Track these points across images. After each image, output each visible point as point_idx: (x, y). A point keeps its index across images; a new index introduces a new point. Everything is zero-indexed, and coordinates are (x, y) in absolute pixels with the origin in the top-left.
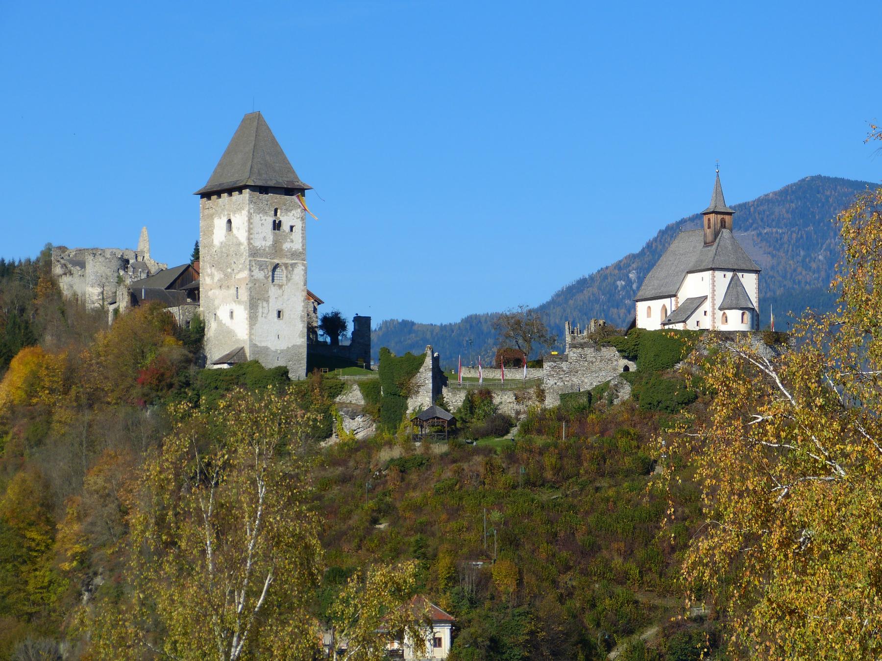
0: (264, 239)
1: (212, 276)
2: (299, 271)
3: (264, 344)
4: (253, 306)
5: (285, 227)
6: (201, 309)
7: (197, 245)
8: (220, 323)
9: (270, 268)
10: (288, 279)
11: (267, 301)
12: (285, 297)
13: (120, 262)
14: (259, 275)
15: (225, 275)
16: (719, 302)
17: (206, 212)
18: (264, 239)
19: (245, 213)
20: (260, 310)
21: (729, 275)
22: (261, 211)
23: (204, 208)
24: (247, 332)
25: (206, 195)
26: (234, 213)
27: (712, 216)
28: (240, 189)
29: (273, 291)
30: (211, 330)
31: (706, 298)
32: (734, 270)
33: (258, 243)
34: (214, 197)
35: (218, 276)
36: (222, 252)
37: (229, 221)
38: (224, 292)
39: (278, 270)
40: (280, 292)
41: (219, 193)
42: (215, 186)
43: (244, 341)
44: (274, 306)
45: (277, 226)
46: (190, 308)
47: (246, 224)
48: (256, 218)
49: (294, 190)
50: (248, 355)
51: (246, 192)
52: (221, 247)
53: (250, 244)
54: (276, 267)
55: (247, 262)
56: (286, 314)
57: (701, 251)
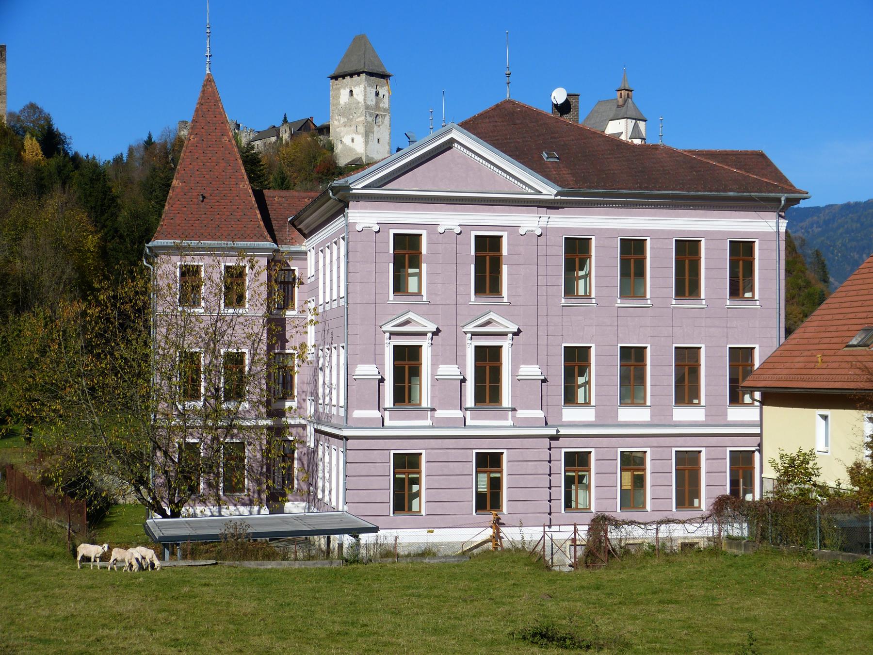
0: (372, 100)
1: (339, 121)
2: (387, 118)
3: (372, 156)
4: (368, 134)
5: (381, 95)
6: (331, 138)
7: (285, 115)
8: (345, 145)
9: (375, 116)
10: (383, 123)
11: (373, 134)
12: (381, 132)
13: (235, 125)
14: (370, 119)
15: (348, 120)
16: (629, 135)
17: (335, 87)
18: (372, 100)
19: (362, 86)
20: (370, 138)
21: (634, 121)
22: (370, 85)
23: (333, 85)
24: (364, 149)
25: (335, 78)
26: (355, 87)
27: (623, 92)
28: (359, 74)
29: (376, 128)
30: (338, 149)
31: (622, 133)
32: (635, 119)
33: (369, 103)
34: (340, 79)
35: (343, 120)
36: (346, 108)
37: (351, 91)
38: (347, 129)
39: (378, 117)
40: (379, 129)
41: (344, 77)
42: (342, 71)
43: (362, 154)
44: (376, 135)
45: (377, 94)
46: (326, 137)
47: (363, 92)
48: (368, 89)
49: (384, 76)
50: (364, 161)
51: (363, 76)
52: (345, 105)
53: (365, 102)
54: (377, 115)
55: (364, 112)
56: (381, 141)
57: (616, 110)
